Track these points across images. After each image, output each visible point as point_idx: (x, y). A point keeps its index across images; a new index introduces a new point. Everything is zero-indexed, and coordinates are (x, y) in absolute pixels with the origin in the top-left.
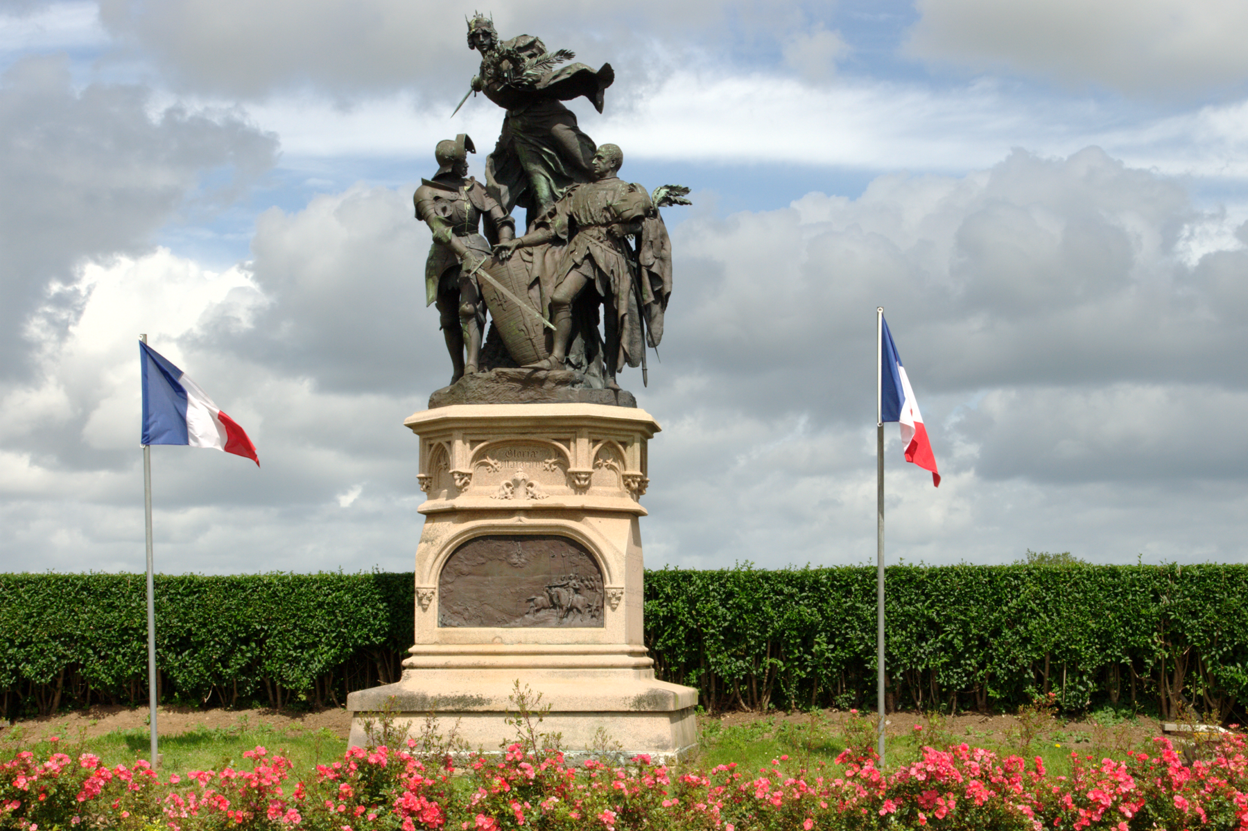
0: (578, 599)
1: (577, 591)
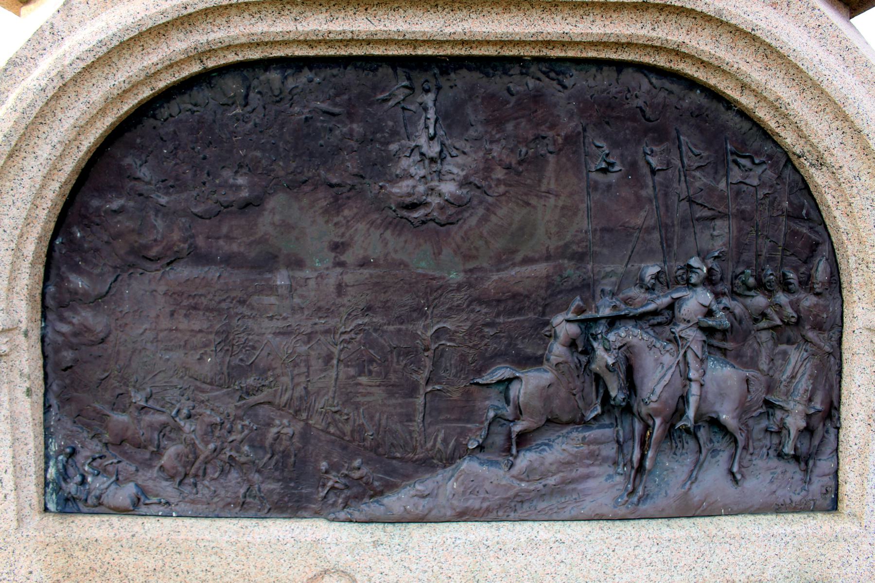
0: (721, 384)
1: (717, 339)
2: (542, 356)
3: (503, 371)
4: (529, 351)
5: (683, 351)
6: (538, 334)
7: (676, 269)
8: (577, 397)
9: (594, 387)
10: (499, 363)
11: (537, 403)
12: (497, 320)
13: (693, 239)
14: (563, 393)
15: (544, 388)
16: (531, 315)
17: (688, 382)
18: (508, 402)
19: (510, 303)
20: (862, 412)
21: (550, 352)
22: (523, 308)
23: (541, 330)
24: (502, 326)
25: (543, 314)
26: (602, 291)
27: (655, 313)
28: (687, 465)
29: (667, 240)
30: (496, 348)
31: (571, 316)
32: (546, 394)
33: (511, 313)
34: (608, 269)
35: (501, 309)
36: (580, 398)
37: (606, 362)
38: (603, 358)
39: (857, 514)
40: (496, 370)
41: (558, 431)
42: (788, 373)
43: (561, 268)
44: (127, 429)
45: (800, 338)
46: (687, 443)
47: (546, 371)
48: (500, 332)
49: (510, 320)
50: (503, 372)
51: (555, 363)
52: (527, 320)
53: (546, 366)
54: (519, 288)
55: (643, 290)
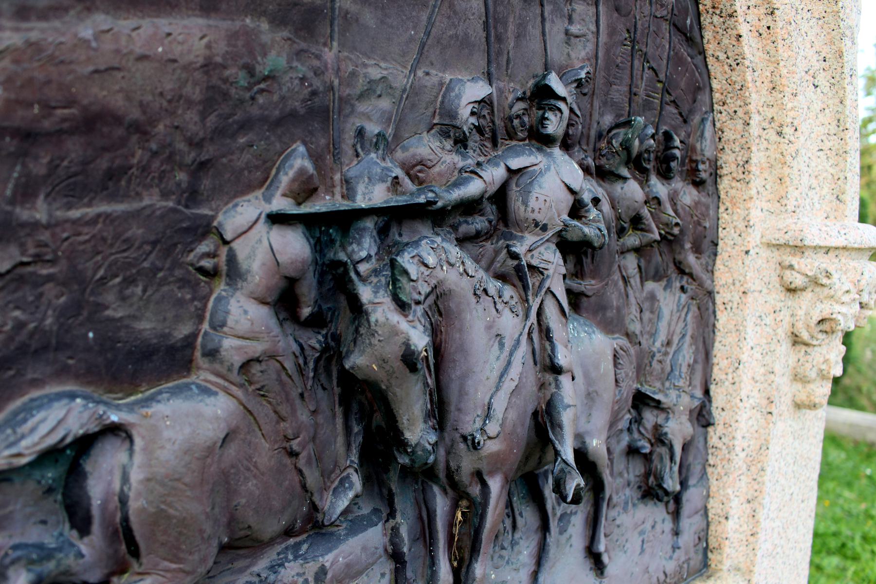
2: (189, 342)
3: (55, 413)
4: (147, 326)
5: (538, 300)
6: (176, 264)
7: (511, 97)
8: (302, 462)
9: (339, 421)
10: (36, 383)
11: (192, 507)
12: (24, 214)
13: (537, 32)
14: (265, 454)
15: (210, 450)
16: (151, 199)
17: (549, 377)
18: (81, 521)
19: (74, 149)
20: (755, 393)
21: (218, 325)
22: (125, 169)
23: (187, 255)
24: (45, 236)
25: (193, 196)
26: (360, 133)
27: (470, 207)
28: (524, 565)
29: (496, 20)
30: (20, 325)
31: (281, 204)
32: (216, 469)
33: (75, 189)
34: (375, 73)
35: (39, 167)
36: (309, 462)
37: (407, 344)
38: (395, 332)
39: (742, 566)
40: (28, 410)
41: (242, 571)
42: (662, 337)
43: (248, 47)
44: (541, 187)
45: (672, 268)
46: (521, 515)
47: (205, 391)
48: (38, 259)
49: (75, 214)
50: (58, 416)
51: (237, 360)
52: (135, 215)
53: (203, 375)
54: (109, 95)
55: (448, 144)
